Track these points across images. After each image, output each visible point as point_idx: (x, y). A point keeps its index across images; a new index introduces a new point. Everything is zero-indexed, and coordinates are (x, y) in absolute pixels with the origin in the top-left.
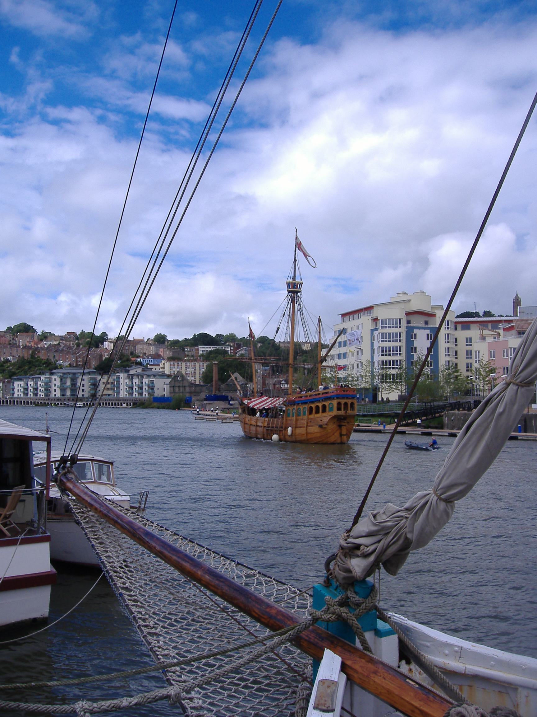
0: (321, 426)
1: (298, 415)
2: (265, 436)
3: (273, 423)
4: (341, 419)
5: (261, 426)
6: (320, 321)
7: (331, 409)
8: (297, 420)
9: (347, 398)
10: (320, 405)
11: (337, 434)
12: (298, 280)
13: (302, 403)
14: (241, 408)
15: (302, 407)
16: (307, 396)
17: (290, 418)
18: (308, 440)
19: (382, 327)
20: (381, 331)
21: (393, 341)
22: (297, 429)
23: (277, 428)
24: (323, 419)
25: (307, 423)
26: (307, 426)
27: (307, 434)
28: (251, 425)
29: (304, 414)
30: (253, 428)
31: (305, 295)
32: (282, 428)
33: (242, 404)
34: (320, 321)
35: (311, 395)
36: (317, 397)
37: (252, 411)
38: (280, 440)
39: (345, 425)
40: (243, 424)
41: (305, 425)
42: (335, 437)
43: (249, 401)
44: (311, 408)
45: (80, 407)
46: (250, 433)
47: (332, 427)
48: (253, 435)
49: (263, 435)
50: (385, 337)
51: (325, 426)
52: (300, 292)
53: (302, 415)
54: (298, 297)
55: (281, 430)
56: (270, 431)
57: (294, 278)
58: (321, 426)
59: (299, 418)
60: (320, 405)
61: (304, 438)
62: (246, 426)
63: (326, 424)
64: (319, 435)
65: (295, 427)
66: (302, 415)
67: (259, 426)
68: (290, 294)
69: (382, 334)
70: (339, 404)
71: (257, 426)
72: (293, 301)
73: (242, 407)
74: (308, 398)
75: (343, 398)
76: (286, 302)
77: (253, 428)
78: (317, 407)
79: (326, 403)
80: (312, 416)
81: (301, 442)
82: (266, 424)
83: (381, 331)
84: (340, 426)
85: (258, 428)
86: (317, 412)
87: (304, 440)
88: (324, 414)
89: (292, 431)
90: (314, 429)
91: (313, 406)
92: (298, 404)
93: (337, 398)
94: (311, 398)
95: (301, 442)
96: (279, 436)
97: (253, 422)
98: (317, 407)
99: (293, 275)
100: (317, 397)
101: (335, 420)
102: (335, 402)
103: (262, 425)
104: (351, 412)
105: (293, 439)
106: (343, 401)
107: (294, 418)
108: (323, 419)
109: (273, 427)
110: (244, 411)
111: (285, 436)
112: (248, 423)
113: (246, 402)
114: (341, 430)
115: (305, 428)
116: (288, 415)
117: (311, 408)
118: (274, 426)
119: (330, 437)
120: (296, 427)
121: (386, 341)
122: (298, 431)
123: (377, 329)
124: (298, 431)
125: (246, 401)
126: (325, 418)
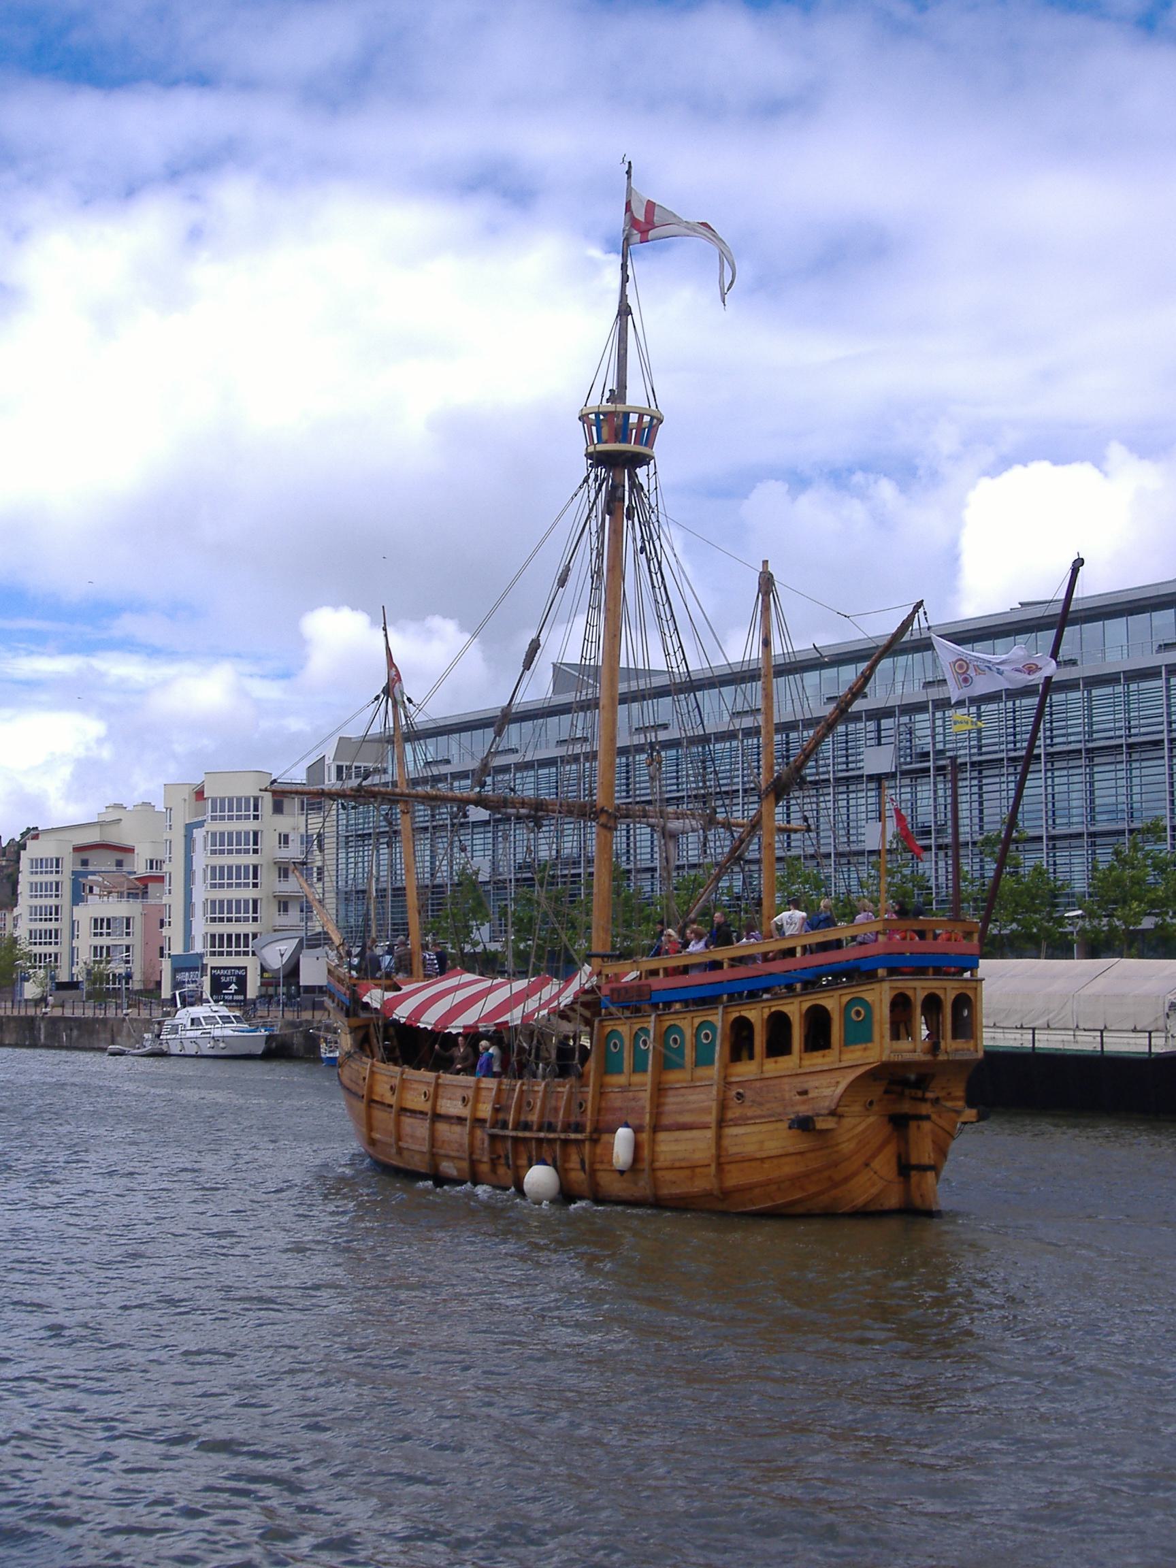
0: (804, 1124)
1: (666, 1063)
2: (485, 1168)
3: (524, 1103)
4: (905, 1083)
5: (460, 1120)
6: (767, 584)
7: (859, 1032)
8: (660, 1090)
9: (938, 971)
10: (795, 1009)
11: (884, 1165)
12: (635, 397)
13: (686, 1003)
14: (353, 1030)
15: (687, 1024)
16: (715, 965)
17: (622, 1079)
18: (726, 1194)
19: (214, 818)
20: (211, 826)
21: (238, 852)
22: (662, 1136)
23: (551, 1128)
24: (810, 1083)
25: (723, 1107)
26: (721, 1123)
27: (721, 1162)
28: (403, 1110)
29: (704, 1058)
30: (417, 1129)
31: (668, 470)
32: (579, 1128)
33: (354, 1007)
34: (767, 584)
35: (737, 961)
36: (778, 967)
37: (414, 1046)
38: (566, 1195)
39: (928, 1118)
40: (361, 1106)
41: (712, 1118)
42: (874, 1181)
43: (389, 995)
44: (742, 1029)
45: (1157, 1031)
46: (400, 1151)
47: (859, 1128)
48: (419, 1163)
49: (473, 1163)
50: (220, 843)
51: (830, 1124)
52: (644, 460)
53: (627, 1064)
54: (636, 487)
55: (573, 1141)
56: (506, 1150)
57: (618, 394)
58: (804, 1124)
59: (673, 1077)
60: (795, 1009)
61: (704, 1183)
62: (379, 1114)
63: (833, 1113)
64: (788, 1168)
65: (654, 1126)
66: (627, 1064)
67: (413, 1112)
68: (602, 472)
69: (214, 835)
70: (901, 1004)
71: (437, 1117)
72: (613, 504)
73: (356, 1022)
74: (726, 974)
75: (919, 971)
76: (580, 506)
77: (417, 1129)
78: (779, 1023)
79: (831, 1003)
80: (745, 1070)
81: (681, 1205)
82: (485, 1110)
83: (211, 826)
84: (900, 1123)
85: (442, 1127)
86: (778, 1045)
87: (708, 1195)
88: (818, 1060)
89: (637, 1147)
90: (762, 1140)
91: (756, 1014)
92: (668, 1005)
93: (893, 971)
94: (742, 971)
95: (681, 1205)
96: (562, 1172)
97: (416, 1100)
98: (779, 1023)
99: (612, 384)
100: (778, 967)
101: (877, 1091)
102: (879, 996)
103: (465, 1112)
104: (960, 1044)
105: (642, 1188)
106: (919, 989)
107: (647, 1078)
108: (810, 1083)
109: (527, 1126)
110: (363, 1043)
111: (593, 1173)
112: (390, 1099)
113: (375, 997)
114: (904, 1140)
115: (710, 1134)
116: (609, 1065)
117: (742, 1029)
118: (534, 1118)
119: (847, 1179)
120: (656, 1128)
121: (222, 852)
122: (671, 1147)
123: (200, 824)
124: (671, 1147)
125: (377, 993)
126: (826, 1078)
